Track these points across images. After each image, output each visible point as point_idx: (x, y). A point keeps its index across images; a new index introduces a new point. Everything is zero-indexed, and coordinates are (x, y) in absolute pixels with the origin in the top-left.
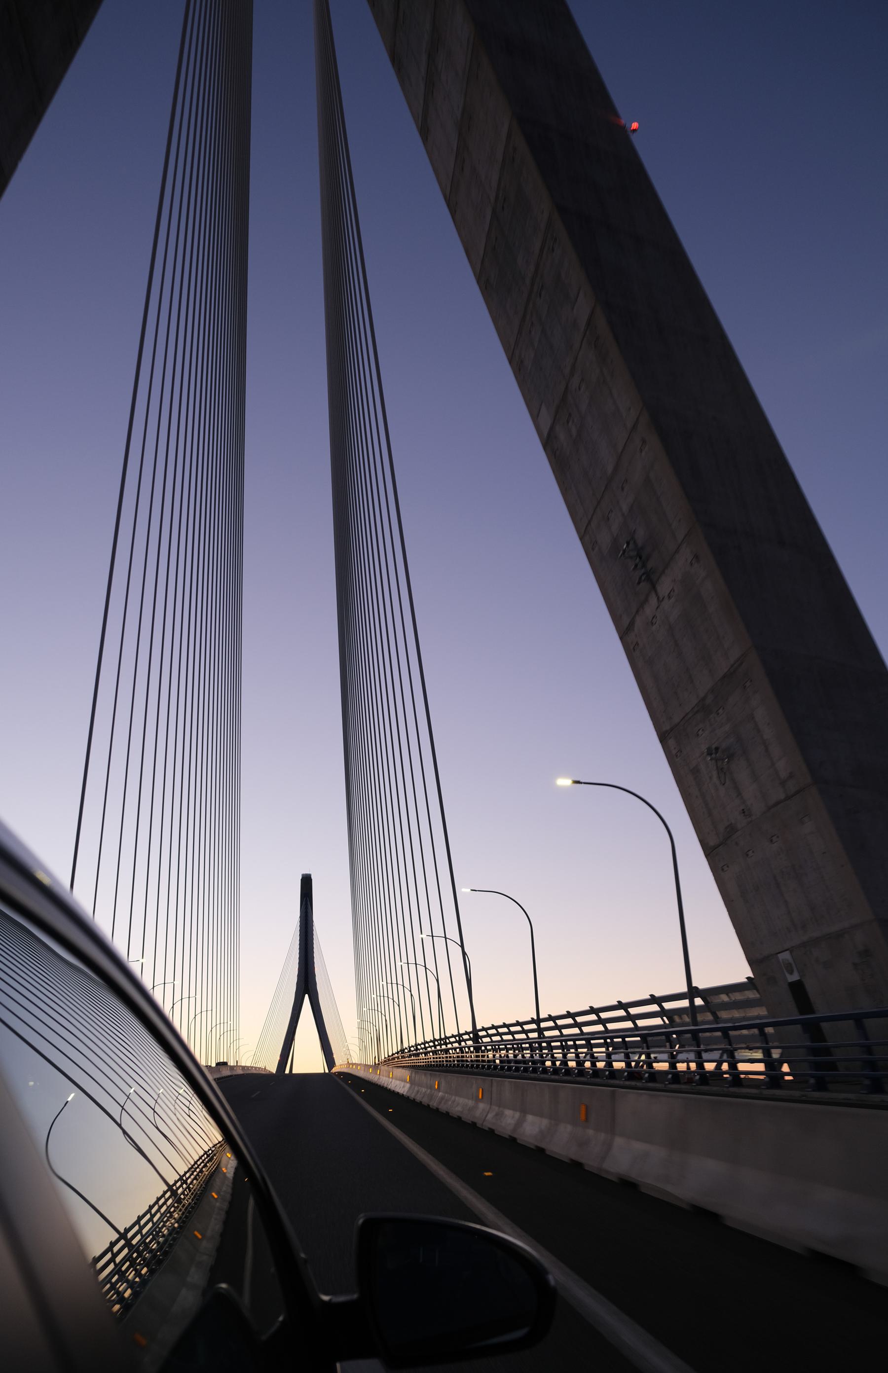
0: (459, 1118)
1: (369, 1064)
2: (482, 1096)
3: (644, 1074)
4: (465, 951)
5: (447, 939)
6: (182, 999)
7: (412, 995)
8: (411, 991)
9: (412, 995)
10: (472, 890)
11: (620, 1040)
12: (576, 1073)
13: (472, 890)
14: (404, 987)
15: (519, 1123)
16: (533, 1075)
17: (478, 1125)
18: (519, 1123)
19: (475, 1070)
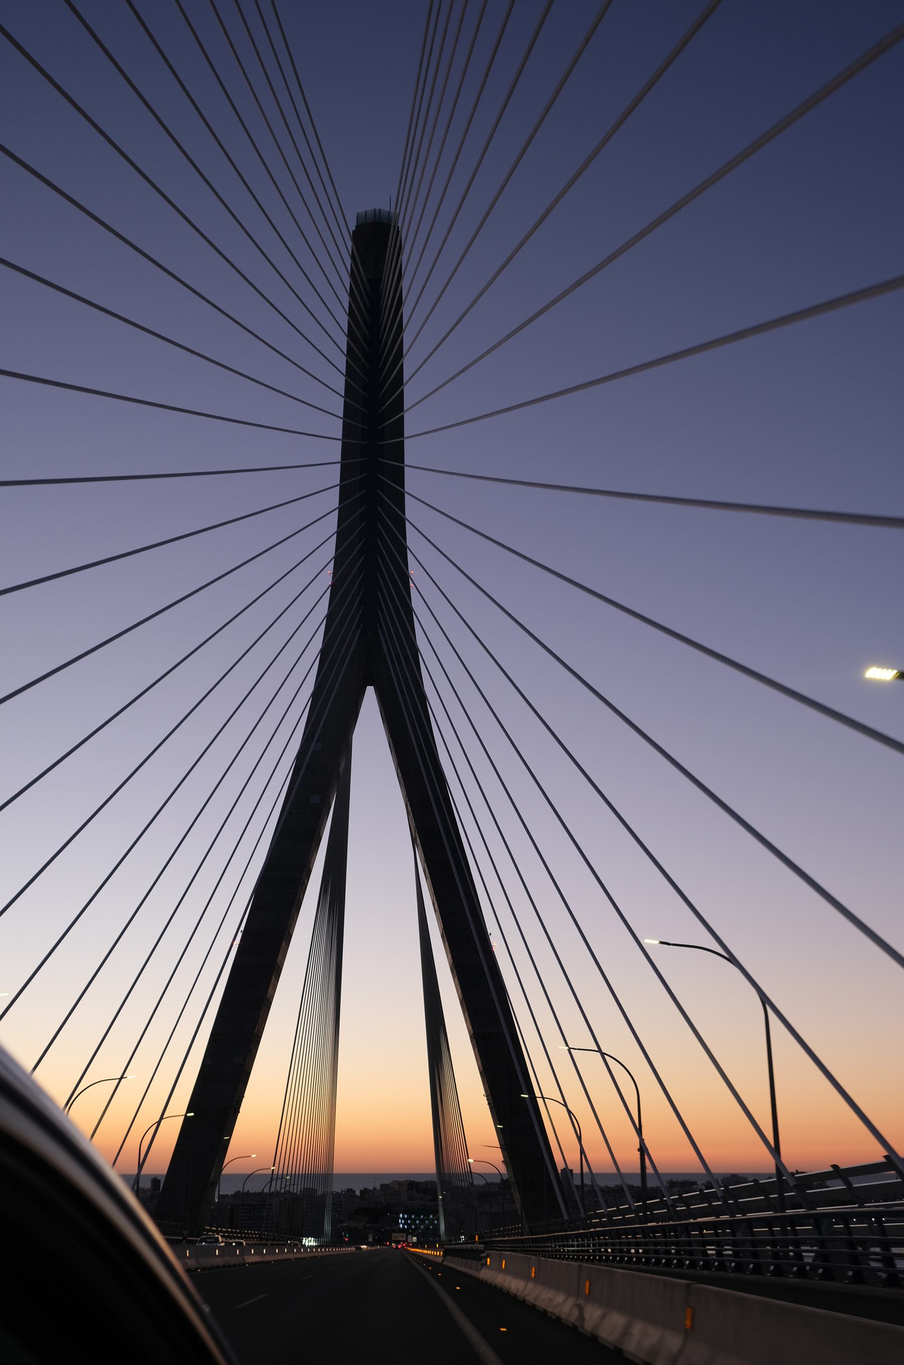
0: (545, 1312)
1: (295, 1191)
2: (589, 1292)
3: (714, 1262)
4: (569, 1108)
5: (545, 1099)
6: (122, 1078)
7: (569, 1112)
8: (565, 1105)
9: (569, 1112)
10: (662, 943)
11: (209, 1233)
12: (701, 1265)
13: (662, 943)
14: (603, 1054)
15: (626, 1332)
16: (655, 1268)
17: (562, 1321)
18: (626, 1332)
19: (732, 1275)
